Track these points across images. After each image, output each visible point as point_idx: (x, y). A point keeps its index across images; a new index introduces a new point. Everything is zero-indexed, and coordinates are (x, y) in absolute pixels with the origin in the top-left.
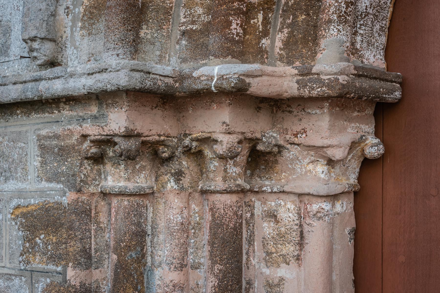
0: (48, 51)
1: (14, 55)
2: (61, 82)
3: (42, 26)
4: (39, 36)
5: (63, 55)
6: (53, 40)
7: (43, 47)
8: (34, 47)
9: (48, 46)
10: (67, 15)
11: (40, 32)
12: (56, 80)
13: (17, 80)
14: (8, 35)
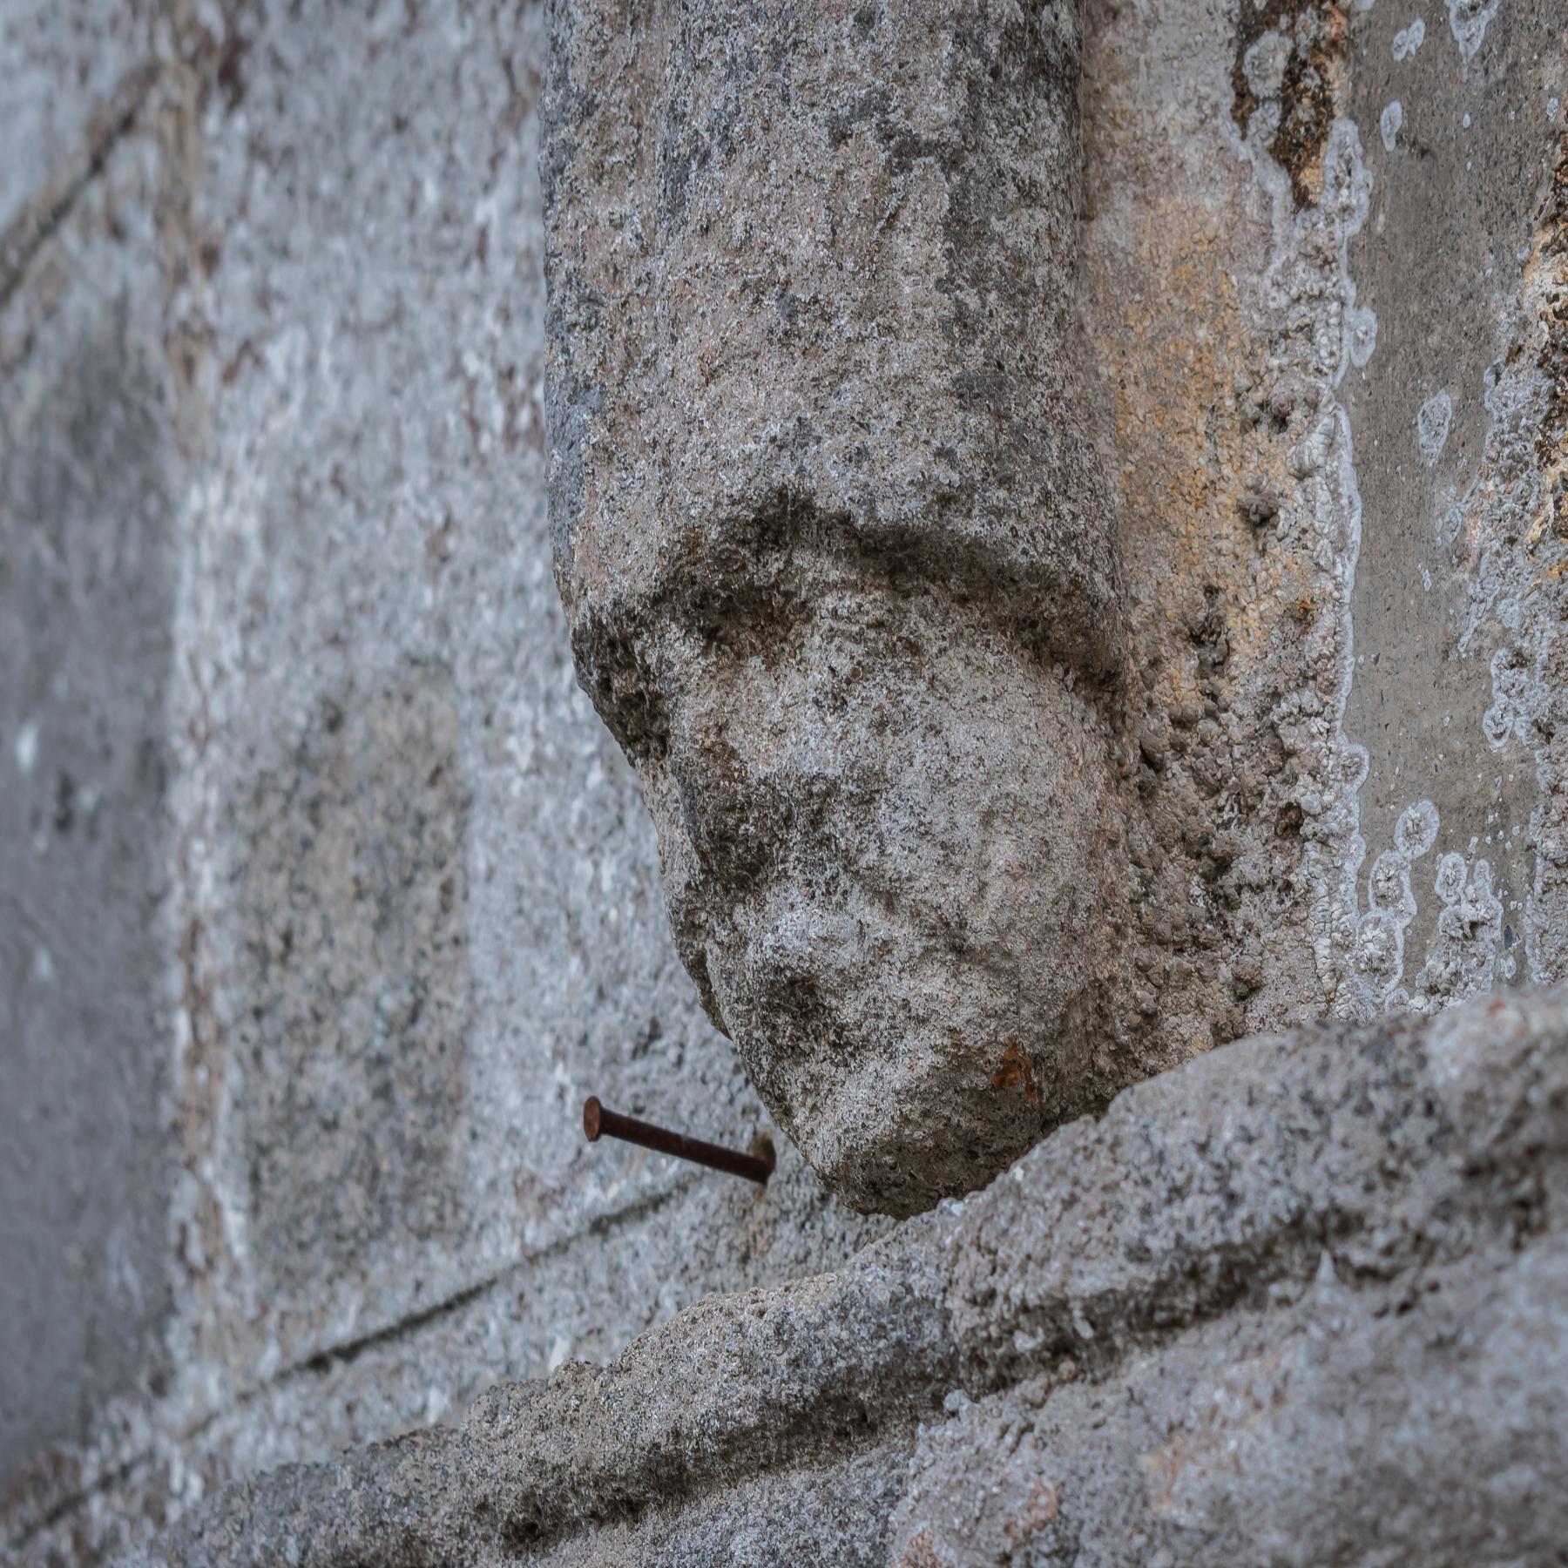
0: (1004, 852)
1: (523, 1185)
2: (1294, 1357)
3: (875, 261)
4: (835, 487)
5: (1246, 989)
6: (1063, 637)
7: (924, 752)
8: (763, 761)
9: (1000, 740)
10: (1291, 151)
11: (851, 396)
12: (1184, 1349)
13: (552, 1452)
14: (429, 893)
